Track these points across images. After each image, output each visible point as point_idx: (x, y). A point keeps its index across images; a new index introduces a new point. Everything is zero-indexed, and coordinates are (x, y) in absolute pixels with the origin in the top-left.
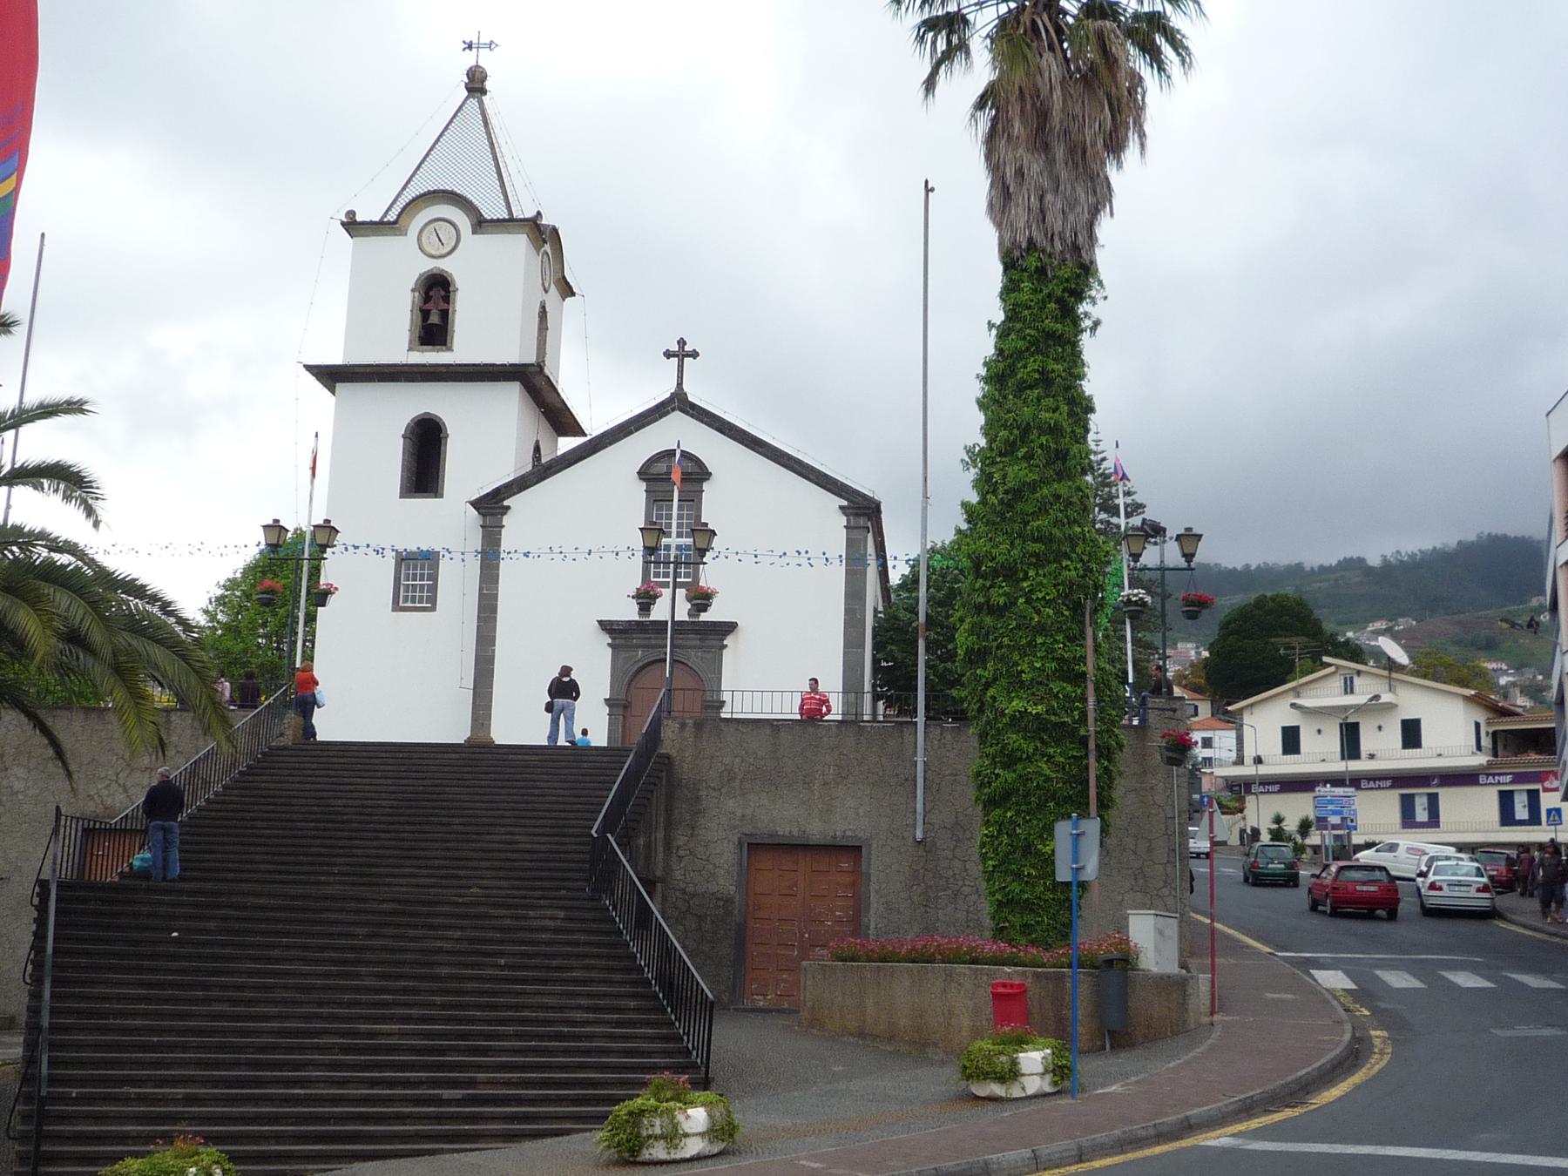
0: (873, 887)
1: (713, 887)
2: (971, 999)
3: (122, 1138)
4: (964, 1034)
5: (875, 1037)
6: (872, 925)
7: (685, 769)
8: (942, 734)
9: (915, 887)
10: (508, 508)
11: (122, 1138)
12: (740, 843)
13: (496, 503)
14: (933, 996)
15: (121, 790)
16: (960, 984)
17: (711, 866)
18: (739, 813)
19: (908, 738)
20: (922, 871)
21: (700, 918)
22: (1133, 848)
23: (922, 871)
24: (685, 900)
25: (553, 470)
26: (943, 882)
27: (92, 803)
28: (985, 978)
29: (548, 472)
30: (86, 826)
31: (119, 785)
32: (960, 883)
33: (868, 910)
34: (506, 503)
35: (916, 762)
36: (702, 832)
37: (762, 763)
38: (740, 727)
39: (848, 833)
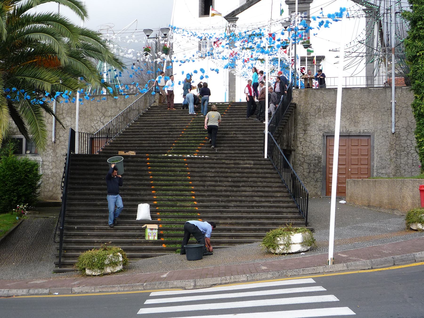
0: (375, 151)
1: (313, 152)
2: (412, 192)
3: (92, 243)
4: (409, 205)
5: (374, 207)
6: (375, 166)
7: (301, 108)
8: (402, 91)
9: (392, 151)
10: (238, 18)
11: (92, 243)
12: (323, 136)
13: (233, 17)
14: (397, 191)
15: (102, 124)
16: (408, 186)
17: (312, 145)
18: (323, 125)
19: (388, 93)
20: (394, 145)
21: (309, 164)
22: (376, 49)
23: (394, 145)
24: (303, 157)
25: (253, 3)
26: (403, 148)
27: (93, 128)
28: (417, 183)
29: (252, 4)
30: (91, 137)
31: (101, 122)
32: (410, 149)
33: (373, 160)
34: (237, 16)
35: (392, 102)
36: (309, 132)
37: (331, 105)
38: (322, 92)
39: (365, 131)
